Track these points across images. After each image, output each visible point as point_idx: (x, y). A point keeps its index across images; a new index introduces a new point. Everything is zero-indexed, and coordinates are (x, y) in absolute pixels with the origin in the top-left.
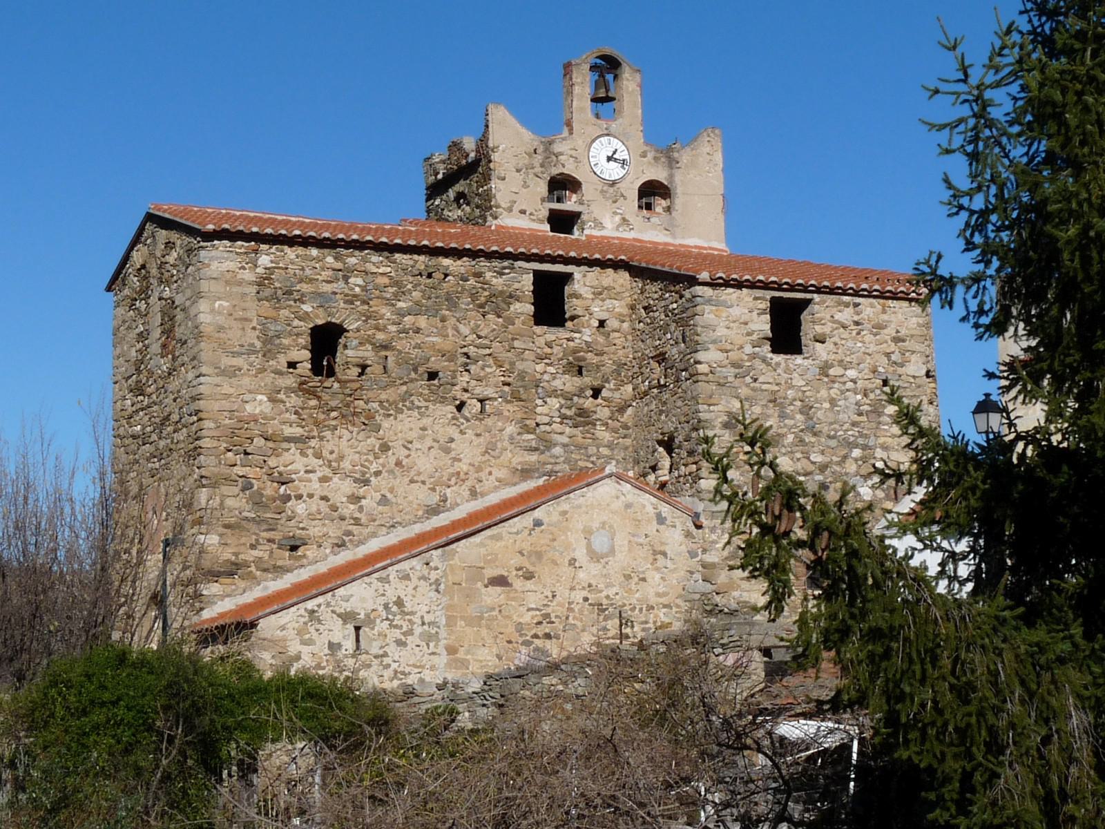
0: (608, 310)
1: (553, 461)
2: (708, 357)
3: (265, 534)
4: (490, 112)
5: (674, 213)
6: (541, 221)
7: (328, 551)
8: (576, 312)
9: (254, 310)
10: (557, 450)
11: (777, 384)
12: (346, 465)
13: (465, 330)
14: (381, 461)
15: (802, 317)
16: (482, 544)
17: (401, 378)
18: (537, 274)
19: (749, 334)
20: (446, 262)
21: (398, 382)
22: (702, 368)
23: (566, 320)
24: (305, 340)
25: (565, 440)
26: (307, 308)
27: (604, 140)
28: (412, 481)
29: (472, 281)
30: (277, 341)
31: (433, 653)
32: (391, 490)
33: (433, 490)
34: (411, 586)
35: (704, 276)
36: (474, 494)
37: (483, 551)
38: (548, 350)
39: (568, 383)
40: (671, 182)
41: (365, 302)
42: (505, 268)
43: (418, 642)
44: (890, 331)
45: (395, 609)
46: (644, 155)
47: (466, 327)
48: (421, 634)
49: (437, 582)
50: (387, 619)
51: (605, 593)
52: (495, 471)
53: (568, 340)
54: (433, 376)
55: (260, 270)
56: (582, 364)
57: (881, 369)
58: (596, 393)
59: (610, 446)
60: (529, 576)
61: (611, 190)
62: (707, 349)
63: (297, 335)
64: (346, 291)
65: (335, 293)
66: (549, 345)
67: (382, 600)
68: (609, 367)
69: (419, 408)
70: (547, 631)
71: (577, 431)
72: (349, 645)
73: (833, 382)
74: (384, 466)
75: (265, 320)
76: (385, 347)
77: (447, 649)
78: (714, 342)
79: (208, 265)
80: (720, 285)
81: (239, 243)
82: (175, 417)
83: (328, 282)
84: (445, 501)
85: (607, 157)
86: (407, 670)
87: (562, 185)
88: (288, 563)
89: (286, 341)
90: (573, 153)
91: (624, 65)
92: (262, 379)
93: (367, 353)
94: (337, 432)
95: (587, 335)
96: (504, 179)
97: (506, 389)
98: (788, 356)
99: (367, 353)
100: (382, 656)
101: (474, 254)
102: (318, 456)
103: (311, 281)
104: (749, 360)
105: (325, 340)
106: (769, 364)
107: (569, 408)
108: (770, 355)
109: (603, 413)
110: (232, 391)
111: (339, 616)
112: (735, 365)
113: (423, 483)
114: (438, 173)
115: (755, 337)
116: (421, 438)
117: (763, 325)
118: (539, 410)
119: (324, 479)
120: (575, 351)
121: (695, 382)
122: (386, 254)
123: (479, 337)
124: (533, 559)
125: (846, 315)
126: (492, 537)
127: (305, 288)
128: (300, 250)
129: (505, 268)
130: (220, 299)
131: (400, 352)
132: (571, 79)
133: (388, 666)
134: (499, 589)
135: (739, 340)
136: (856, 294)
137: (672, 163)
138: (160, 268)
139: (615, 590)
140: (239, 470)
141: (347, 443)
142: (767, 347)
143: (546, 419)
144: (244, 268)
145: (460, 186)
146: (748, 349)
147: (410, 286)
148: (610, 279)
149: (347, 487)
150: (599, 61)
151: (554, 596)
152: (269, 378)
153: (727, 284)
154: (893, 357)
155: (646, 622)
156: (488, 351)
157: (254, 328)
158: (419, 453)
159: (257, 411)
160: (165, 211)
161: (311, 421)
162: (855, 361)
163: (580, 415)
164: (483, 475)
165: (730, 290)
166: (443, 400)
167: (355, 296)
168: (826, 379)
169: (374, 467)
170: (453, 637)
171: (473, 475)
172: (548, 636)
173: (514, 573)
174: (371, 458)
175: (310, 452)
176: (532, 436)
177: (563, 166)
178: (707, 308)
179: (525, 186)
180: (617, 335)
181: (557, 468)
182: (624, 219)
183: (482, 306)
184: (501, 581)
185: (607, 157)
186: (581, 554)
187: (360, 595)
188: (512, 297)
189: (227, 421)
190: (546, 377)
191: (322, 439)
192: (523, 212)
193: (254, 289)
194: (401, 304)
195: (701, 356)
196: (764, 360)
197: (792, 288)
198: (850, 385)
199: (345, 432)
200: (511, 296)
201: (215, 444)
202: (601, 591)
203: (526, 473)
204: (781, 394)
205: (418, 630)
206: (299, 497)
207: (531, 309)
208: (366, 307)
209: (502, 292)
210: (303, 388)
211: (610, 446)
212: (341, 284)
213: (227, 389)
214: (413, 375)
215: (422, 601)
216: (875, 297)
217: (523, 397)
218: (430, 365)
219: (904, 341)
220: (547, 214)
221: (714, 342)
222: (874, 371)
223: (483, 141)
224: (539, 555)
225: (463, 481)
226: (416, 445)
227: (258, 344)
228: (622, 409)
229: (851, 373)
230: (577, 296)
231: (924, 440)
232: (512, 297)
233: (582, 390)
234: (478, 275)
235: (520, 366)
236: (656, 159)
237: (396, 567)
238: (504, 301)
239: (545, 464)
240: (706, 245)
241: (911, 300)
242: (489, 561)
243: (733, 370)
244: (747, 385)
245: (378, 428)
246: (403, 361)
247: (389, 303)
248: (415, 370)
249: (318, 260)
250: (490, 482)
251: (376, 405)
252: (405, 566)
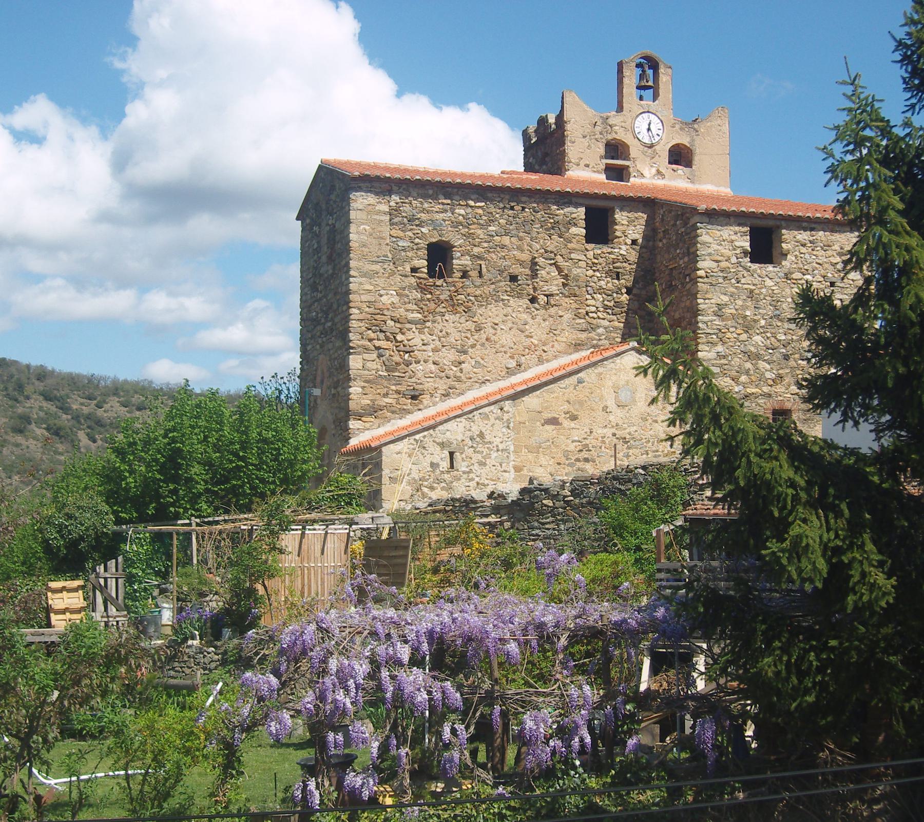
2: (705, 265)
3: (393, 388)
6: (598, 172)
7: (437, 399)
11: (754, 285)
14: (476, 337)
24: (424, 253)
26: (424, 230)
31: (505, 471)
34: (490, 423)
49: (508, 421)
50: (472, 447)
51: (628, 431)
53: (609, 253)
60: (574, 418)
61: (650, 151)
67: (469, 434)
69: (503, 300)
70: (586, 456)
72: (445, 465)
77: (514, 468)
82: (335, 306)
85: (648, 126)
86: (486, 482)
88: (409, 407)
90: (623, 124)
98: (762, 265)
99: (466, 261)
100: (469, 472)
108: (749, 264)
110: (371, 288)
111: (438, 444)
113: (505, 352)
119: (435, 350)
124: (577, 406)
127: (423, 216)
130: (363, 224)
133: (472, 479)
134: (553, 427)
135: (727, 253)
138: (327, 203)
139: (635, 428)
141: (452, 325)
143: (594, 309)
149: (452, 355)
150: (642, 60)
151: (591, 432)
155: (657, 451)
157: (387, 244)
166: (520, 296)
169: (471, 342)
170: (519, 460)
172: (586, 460)
173: (564, 416)
181: (600, 343)
184: (554, 421)
185: (648, 126)
186: (611, 404)
187: (455, 431)
188: (572, 223)
193: (388, 217)
202: (625, 429)
204: (757, 291)
206: (418, 362)
215: (497, 433)
218: (511, 271)
220: (604, 167)
223: (560, 118)
224: (581, 403)
231: (868, 264)
236: (681, 129)
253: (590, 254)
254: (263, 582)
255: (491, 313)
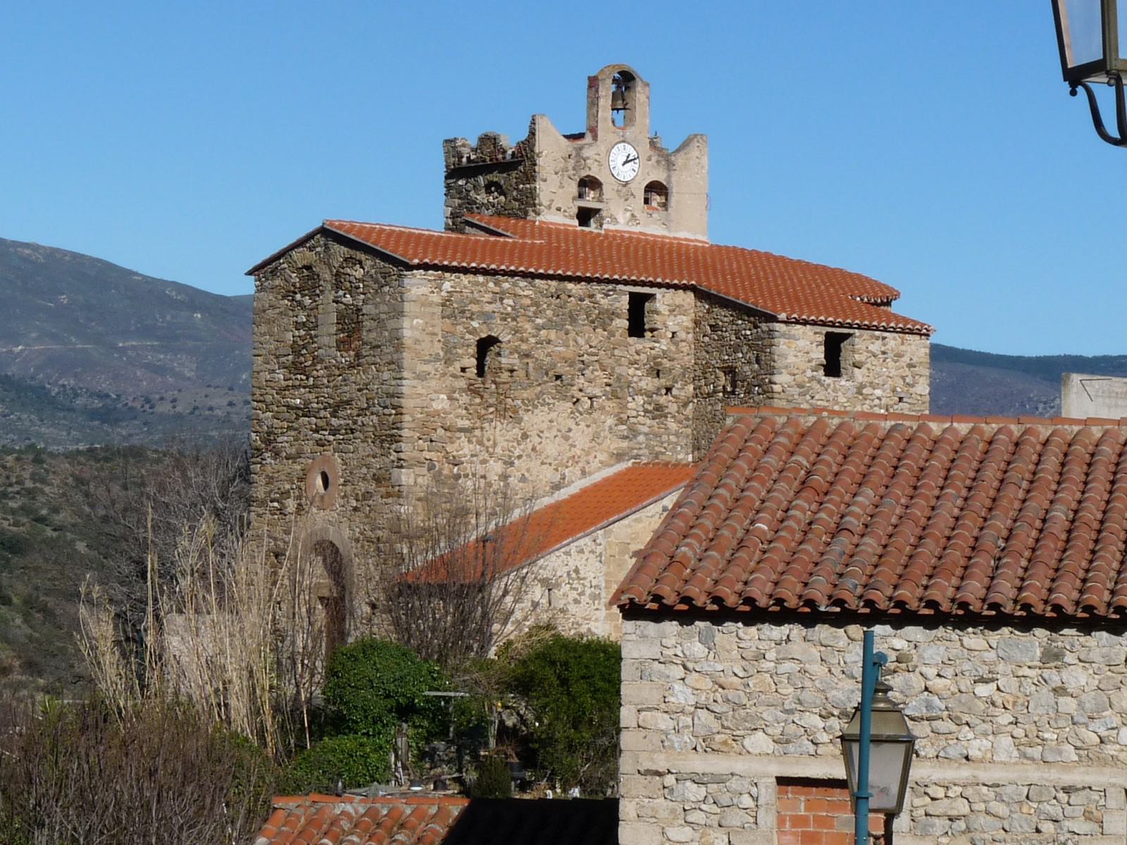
0: (678, 324)
1: (637, 446)
2: (782, 379)
4: (537, 121)
5: (670, 210)
6: (571, 217)
8: (656, 326)
9: (439, 325)
10: (641, 438)
12: (499, 450)
13: (581, 341)
14: (522, 447)
15: (842, 345)
16: (629, 526)
17: (537, 381)
18: (631, 294)
19: (809, 361)
20: (570, 286)
21: (535, 383)
22: (777, 388)
23: (645, 330)
25: (645, 429)
26: (475, 324)
27: (621, 146)
28: (543, 463)
29: (587, 302)
30: (454, 351)
32: (528, 470)
33: (557, 470)
35: (783, 316)
36: (584, 473)
37: (629, 530)
38: (637, 357)
39: (648, 383)
40: (669, 183)
41: (514, 319)
42: (609, 290)
43: (588, 600)
44: (906, 359)
45: (574, 575)
46: (649, 159)
47: (587, 339)
48: (590, 595)
49: (600, 555)
52: (599, 455)
54: (558, 377)
55: (444, 294)
56: (660, 368)
57: (899, 389)
58: (669, 390)
59: (677, 434)
61: (624, 189)
62: (781, 373)
63: (468, 346)
64: (502, 310)
65: (494, 312)
66: (638, 353)
67: (566, 569)
68: (678, 370)
69: (548, 404)
71: (654, 423)
73: (865, 399)
74: (523, 451)
75: (447, 334)
76: (527, 356)
78: (786, 367)
79: (410, 290)
80: (792, 323)
81: (431, 272)
83: (490, 303)
84: (564, 479)
85: (622, 163)
87: (589, 183)
89: (460, 351)
90: (597, 157)
91: (637, 79)
92: (444, 382)
93: (514, 361)
94: (493, 424)
95: (664, 345)
96: (545, 180)
97: (608, 388)
99: (514, 361)
101: (589, 280)
102: (480, 443)
103: (478, 302)
104: (809, 382)
105: (485, 345)
106: (822, 385)
107: (650, 404)
108: (824, 378)
109: (673, 408)
110: (423, 391)
112: (800, 386)
113: (550, 464)
114: (462, 157)
115: (814, 363)
116: (549, 428)
117: (819, 354)
118: (630, 405)
120: (655, 358)
121: (768, 398)
122: (529, 280)
123: (591, 347)
125: (876, 347)
126: (636, 520)
127: (475, 308)
128: (471, 277)
129: (609, 290)
131: (537, 359)
132: (597, 91)
135: (803, 366)
136: (885, 330)
137: (670, 165)
140: (428, 455)
141: (501, 433)
142: (822, 372)
143: (634, 413)
144: (433, 292)
145: (495, 177)
146: (809, 373)
147: (545, 306)
148: (680, 299)
152: (449, 381)
153: (797, 322)
154: (908, 380)
156: (596, 358)
158: (548, 441)
159: (440, 408)
160: (336, 227)
161: (475, 415)
162: (881, 383)
163: (657, 410)
164: (591, 458)
165: (798, 326)
166: (565, 398)
167: (507, 314)
168: (861, 397)
171: (584, 459)
174: (515, 444)
175: (474, 440)
176: (625, 427)
177: (590, 169)
178: (782, 340)
179: (562, 187)
180: (684, 344)
182: (633, 215)
183: (593, 322)
188: (614, 314)
189: (419, 416)
190: (635, 379)
191: (482, 429)
192: (559, 209)
194: (539, 321)
195: (776, 378)
196: (819, 382)
197: (842, 326)
198: (877, 402)
199: (498, 423)
200: (613, 313)
201: (412, 433)
203: (619, 457)
205: (588, 591)
206: (466, 476)
207: (626, 323)
208: (515, 323)
209: (607, 310)
210: (472, 390)
211: (677, 434)
212: (498, 303)
213: (420, 390)
214: (545, 378)
216: (897, 332)
217: (620, 395)
219: (915, 367)
220: (576, 211)
221: (786, 367)
222: (894, 391)
225: (577, 462)
226: (546, 434)
227: (442, 354)
228: (685, 405)
229: (878, 392)
230: (657, 313)
232: (614, 314)
233: (659, 389)
234: (592, 296)
235: (618, 370)
236: (658, 162)
237: (576, 544)
238: (608, 317)
239: (633, 449)
240: (693, 238)
241: (921, 335)
242: (633, 539)
243: (798, 390)
244: (807, 402)
245: (520, 421)
246: (539, 368)
247: (530, 320)
248: (547, 374)
249: (482, 284)
250: (595, 464)
251: (519, 402)
252: (581, 542)
253: (632, 350)
254: (912, 719)
255: (535, 419)
